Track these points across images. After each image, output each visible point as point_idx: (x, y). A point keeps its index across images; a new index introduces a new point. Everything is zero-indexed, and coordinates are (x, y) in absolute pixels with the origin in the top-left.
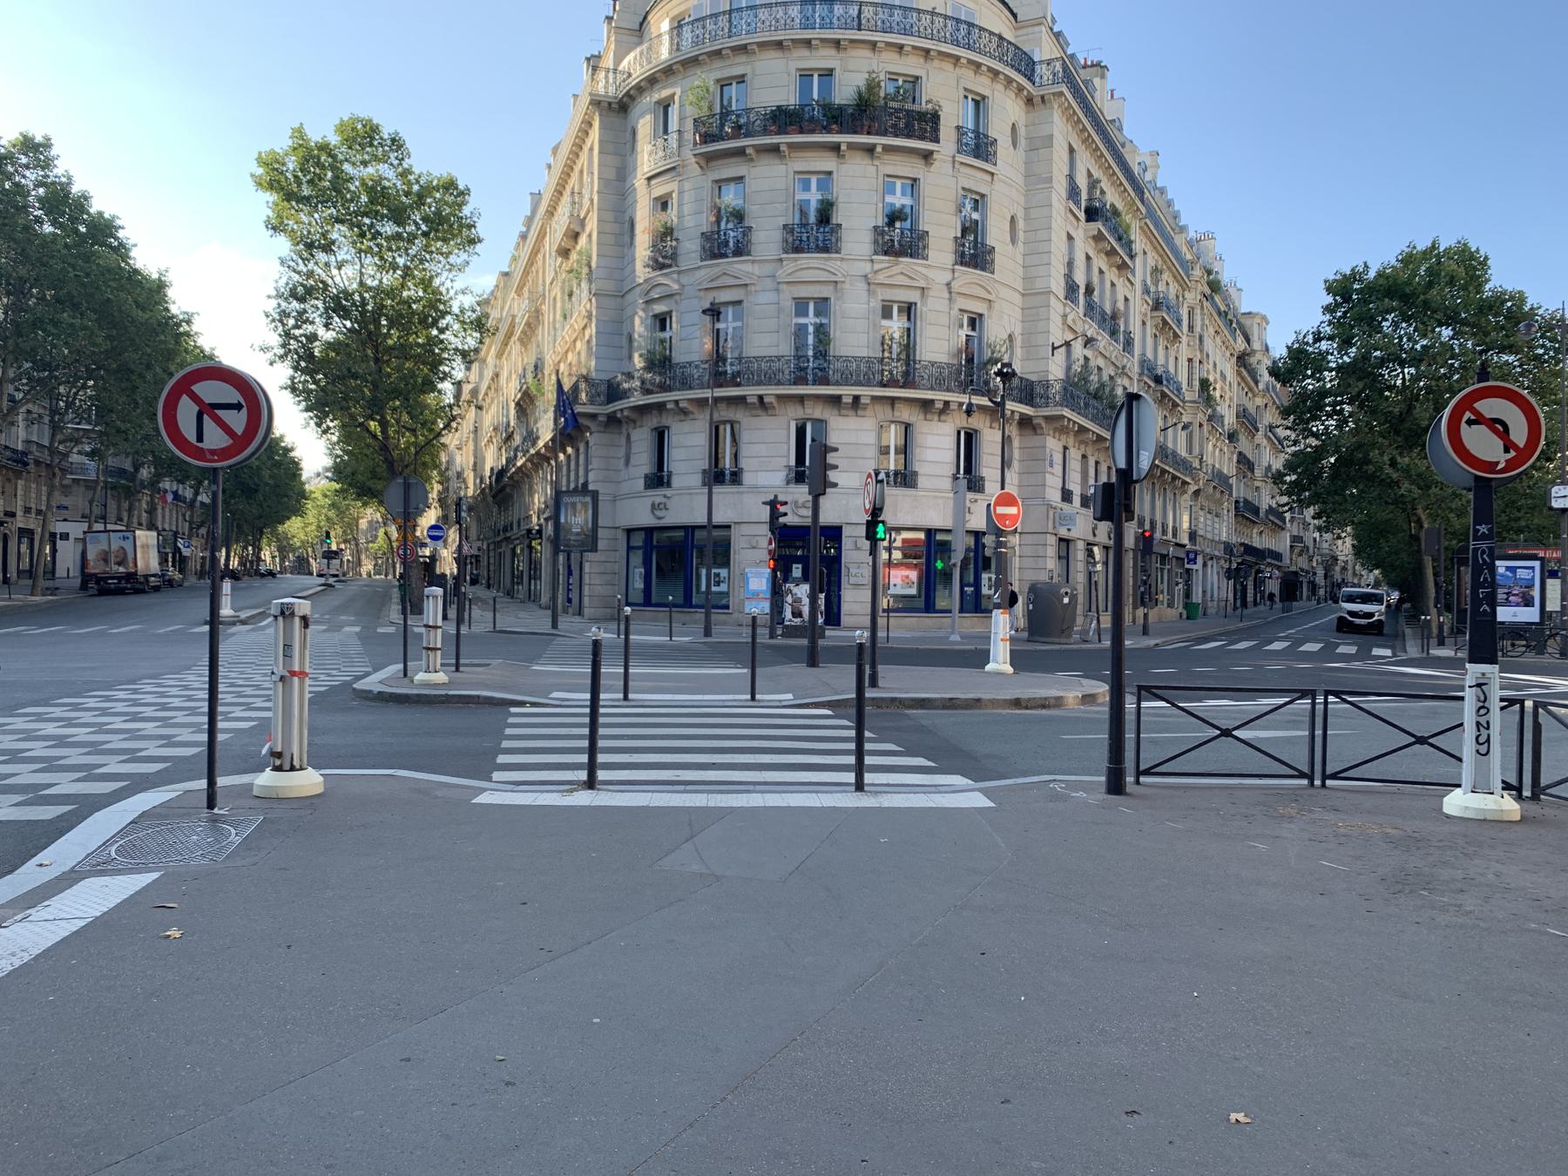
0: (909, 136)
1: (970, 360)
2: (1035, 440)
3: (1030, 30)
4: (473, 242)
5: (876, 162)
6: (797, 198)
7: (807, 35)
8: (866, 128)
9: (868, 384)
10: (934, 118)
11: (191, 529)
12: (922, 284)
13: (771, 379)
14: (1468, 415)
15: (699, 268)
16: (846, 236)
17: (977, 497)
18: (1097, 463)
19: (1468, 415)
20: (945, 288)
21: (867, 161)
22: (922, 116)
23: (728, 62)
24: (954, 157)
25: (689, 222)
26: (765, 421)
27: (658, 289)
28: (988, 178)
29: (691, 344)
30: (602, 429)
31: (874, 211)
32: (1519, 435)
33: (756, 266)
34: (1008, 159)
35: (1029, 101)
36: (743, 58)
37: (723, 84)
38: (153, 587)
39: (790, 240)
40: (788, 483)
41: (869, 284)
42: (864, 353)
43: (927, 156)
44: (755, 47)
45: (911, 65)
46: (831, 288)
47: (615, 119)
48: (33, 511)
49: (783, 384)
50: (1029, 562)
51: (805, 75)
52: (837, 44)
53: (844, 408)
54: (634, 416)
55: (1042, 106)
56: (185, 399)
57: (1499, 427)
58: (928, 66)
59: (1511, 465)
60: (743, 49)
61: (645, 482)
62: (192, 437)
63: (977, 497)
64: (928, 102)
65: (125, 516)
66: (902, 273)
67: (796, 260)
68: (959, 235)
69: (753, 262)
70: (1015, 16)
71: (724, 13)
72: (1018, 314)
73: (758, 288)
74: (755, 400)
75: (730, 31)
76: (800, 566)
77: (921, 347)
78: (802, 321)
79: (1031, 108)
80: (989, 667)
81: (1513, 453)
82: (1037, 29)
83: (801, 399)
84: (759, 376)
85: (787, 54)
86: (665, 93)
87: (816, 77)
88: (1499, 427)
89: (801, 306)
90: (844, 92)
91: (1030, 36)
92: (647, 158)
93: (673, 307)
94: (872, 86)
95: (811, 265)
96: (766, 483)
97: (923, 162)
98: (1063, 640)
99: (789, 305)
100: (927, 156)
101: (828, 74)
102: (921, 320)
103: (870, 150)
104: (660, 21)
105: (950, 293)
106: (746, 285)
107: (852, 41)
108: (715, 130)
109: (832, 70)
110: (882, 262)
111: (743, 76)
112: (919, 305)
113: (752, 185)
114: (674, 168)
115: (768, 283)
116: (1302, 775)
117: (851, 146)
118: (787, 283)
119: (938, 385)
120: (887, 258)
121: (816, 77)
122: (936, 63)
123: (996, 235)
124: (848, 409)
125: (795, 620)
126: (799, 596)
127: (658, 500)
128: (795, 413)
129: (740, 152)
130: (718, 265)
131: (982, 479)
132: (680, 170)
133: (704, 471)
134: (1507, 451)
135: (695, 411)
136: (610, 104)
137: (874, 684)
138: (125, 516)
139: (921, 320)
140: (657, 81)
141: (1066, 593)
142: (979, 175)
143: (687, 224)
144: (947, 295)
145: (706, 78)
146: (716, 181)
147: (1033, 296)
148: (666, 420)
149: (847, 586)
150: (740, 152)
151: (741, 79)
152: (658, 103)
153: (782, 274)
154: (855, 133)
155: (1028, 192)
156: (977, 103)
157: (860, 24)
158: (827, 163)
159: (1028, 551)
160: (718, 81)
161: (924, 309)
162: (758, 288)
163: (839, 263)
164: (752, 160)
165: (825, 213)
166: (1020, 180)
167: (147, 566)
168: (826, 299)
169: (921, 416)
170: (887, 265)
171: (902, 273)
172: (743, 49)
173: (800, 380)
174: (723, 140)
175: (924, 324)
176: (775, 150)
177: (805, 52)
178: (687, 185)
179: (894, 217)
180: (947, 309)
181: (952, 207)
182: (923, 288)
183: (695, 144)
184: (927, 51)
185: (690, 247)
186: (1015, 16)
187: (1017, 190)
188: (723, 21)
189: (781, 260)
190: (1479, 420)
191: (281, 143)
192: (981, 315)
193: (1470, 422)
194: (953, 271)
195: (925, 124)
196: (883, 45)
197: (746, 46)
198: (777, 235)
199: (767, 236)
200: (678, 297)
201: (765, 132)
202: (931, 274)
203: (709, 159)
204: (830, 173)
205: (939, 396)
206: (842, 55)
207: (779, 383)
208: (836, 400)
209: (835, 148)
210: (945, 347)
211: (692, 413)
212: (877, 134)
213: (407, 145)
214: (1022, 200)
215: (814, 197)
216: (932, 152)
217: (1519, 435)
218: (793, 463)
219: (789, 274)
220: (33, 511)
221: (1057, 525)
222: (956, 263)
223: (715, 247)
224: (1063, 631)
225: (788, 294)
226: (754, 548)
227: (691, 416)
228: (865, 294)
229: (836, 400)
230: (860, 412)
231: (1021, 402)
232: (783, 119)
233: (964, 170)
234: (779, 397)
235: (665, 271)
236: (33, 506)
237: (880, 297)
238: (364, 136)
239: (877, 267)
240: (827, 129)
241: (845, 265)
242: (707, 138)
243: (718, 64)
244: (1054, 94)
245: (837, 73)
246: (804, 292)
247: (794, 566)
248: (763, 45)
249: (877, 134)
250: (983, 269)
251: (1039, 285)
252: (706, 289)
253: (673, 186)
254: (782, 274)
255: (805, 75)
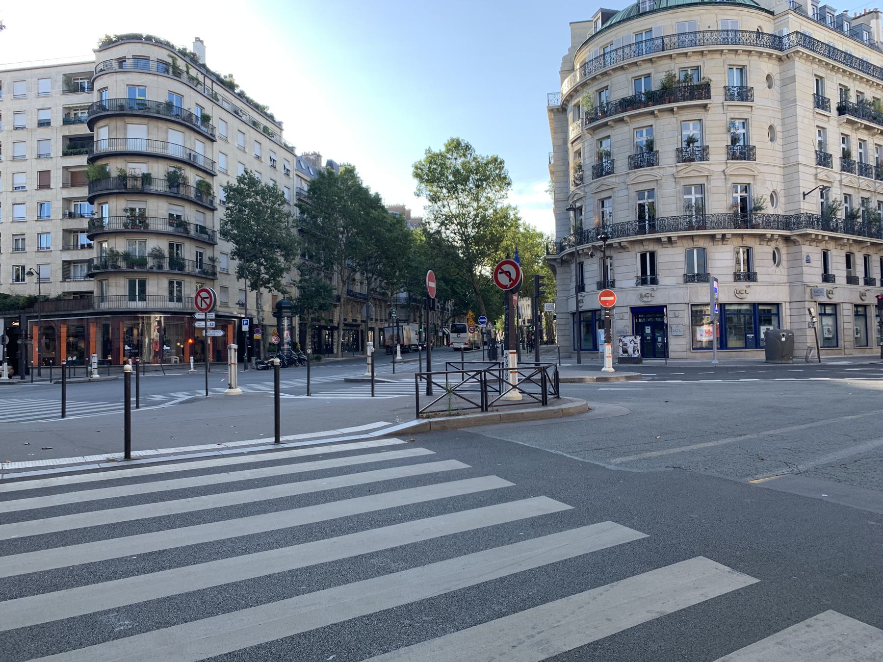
0: (692, 99)
1: (743, 209)
2: (794, 249)
3: (782, 18)
4: (509, 184)
5: (675, 116)
6: (636, 141)
7: (621, 64)
8: (668, 100)
9: (676, 230)
10: (707, 86)
11: (442, 324)
12: (706, 173)
13: (625, 233)
14: (500, 271)
15: (592, 183)
16: (661, 156)
17: (750, 284)
18: (866, 259)
19: (500, 271)
20: (722, 173)
21: (671, 116)
22: (699, 87)
23: (601, 81)
24: (723, 103)
25: (588, 161)
26: (625, 255)
27: (576, 196)
28: (749, 109)
29: (591, 221)
30: (560, 265)
31: (676, 141)
32: (514, 276)
33: (617, 178)
34: (761, 94)
35: (780, 59)
36: (607, 78)
37: (600, 92)
38: (413, 350)
39: (633, 162)
40: (637, 285)
41: (675, 178)
42: (674, 214)
43: (705, 106)
44: (627, 66)
45: (694, 61)
46: (655, 183)
47: (561, 116)
48: (374, 319)
49: (630, 236)
50: (796, 319)
51: (637, 79)
52: (651, 60)
53: (664, 244)
54: (569, 258)
55: (788, 60)
56: (199, 297)
57: (508, 274)
58: (704, 59)
59: (511, 285)
60: (605, 74)
61: (598, 286)
62: (200, 306)
63: (750, 284)
64: (703, 78)
65: (418, 319)
66: (694, 170)
67: (635, 172)
68: (730, 143)
69: (616, 176)
70: (772, 13)
71: (601, 56)
72: (779, 178)
73: (618, 189)
74: (617, 245)
75: (604, 64)
76: (649, 327)
77: (708, 207)
78: (650, 201)
79: (782, 63)
80: (603, 369)
81: (512, 282)
82: (786, 17)
83: (641, 242)
84: (618, 233)
85: (627, 71)
86: (576, 101)
87: (643, 79)
88: (508, 274)
89: (640, 194)
90: (656, 86)
91: (782, 22)
92: (573, 131)
93: (583, 204)
94: (670, 77)
95: (645, 174)
96: (627, 286)
97: (704, 110)
98: (783, 362)
99: (634, 195)
100: (705, 106)
101: (648, 76)
102: (708, 193)
103: (671, 110)
104: (577, 64)
105: (725, 175)
106: (613, 188)
107: (658, 58)
108: (593, 116)
109: (650, 74)
110: (682, 166)
111: (607, 86)
112: (706, 185)
113: (614, 138)
114: (580, 137)
115: (623, 186)
116: (497, 391)
117: (660, 111)
118: (632, 184)
119: (718, 226)
120: (684, 163)
121: (643, 79)
122: (709, 56)
123: (757, 138)
124: (667, 244)
125: (624, 355)
126: (626, 342)
127: (739, 289)
128: (640, 249)
129: (606, 125)
130: (599, 181)
131: (756, 273)
132: (583, 137)
133: (598, 283)
134: (510, 281)
135: (630, 247)
136: (558, 109)
137: (511, 372)
138: (418, 319)
139: (708, 193)
140: (578, 91)
141: (783, 335)
142: (742, 109)
143: (587, 163)
144: (723, 177)
145: (590, 91)
146: (599, 140)
147: (790, 168)
148: (583, 259)
149: (671, 337)
150: (606, 125)
151: (606, 88)
152: (575, 106)
153: (629, 180)
154: (662, 104)
155: (783, 109)
156: (741, 70)
157: (663, 48)
158: (649, 121)
159: (795, 312)
160: (597, 91)
161: (709, 186)
162: (618, 189)
163: (658, 170)
164: (612, 127)
165: (650, 145)
166: (777, 105)
167: (409, 340)
168: (653, 189)
169: (711, 243)
170: (683, 168)
171: (694, 170)
172: (605, 74)
173: (691, 228)
174: (598, 120)
175: (709, 194)
176: (621, 120)
177: (635, 68)
178: (586, 144)
179: (691, 141)
180: (724, 184)
181: (724, 130)
182: (707, 176)
183: (586, 124)
184: (702, 52)
185: (588, 173)
186: (772, 13)
187: (773, 110)
188: (634, 47)
189: (628, 174)
190: (503, 272)
191: (422, 157)
192: (749, 184)
193: (500, 273)
194: (727, 163)
195: (702, 90)
196: (675, 55)
197: (606, 72)
198: (626, 161)
199: (621, 163)
200: (584, 199)
201: (616, 112)
202: (712, 167)
203: (594, 129)
204: (651, 126)
205: (719, 232)
206: (655, 65)
207: (628, 235)
208: (658, 240)
209: (652, 113)
210: (724, 204)
211: (628, 248)
212: (674, 102)
213: (473, 147)
214: (779, 115)
215: (644, 139)
216: (707, 105)
217: (514, 276)
218: (639, 274)
219: (633, 180)
220: (374, 319)
221: (813, 296)
222: (728, 159)
223: (600, 171)
224: (783, 357)
225: (633, 190)
226: (622, 319)
227: (627, 250)
228: (674, 184)
229: (713, 237)
230: (724, 243)
231: (783, 229)
232: (627, 104)
233: (730, 108)
234: (679, 237)
235: (578, 187)
236: (379, 318)
237: (682, 184)
238: (456, 146)
239: (679, 169)
240: (647, 106)
241: (662, 171)
242: (591, 120)
243: (596, 83)
244: (794, 52)
245: (652, 75)
246: (641, 187)
247: (646, 327)
248: (614, 70)
249: (673, 102)
250: (749, 159)
251: (792, 160)
252: (595, 193)
253: (580, 145)
254: (629, 180)
255: (637, 79)
